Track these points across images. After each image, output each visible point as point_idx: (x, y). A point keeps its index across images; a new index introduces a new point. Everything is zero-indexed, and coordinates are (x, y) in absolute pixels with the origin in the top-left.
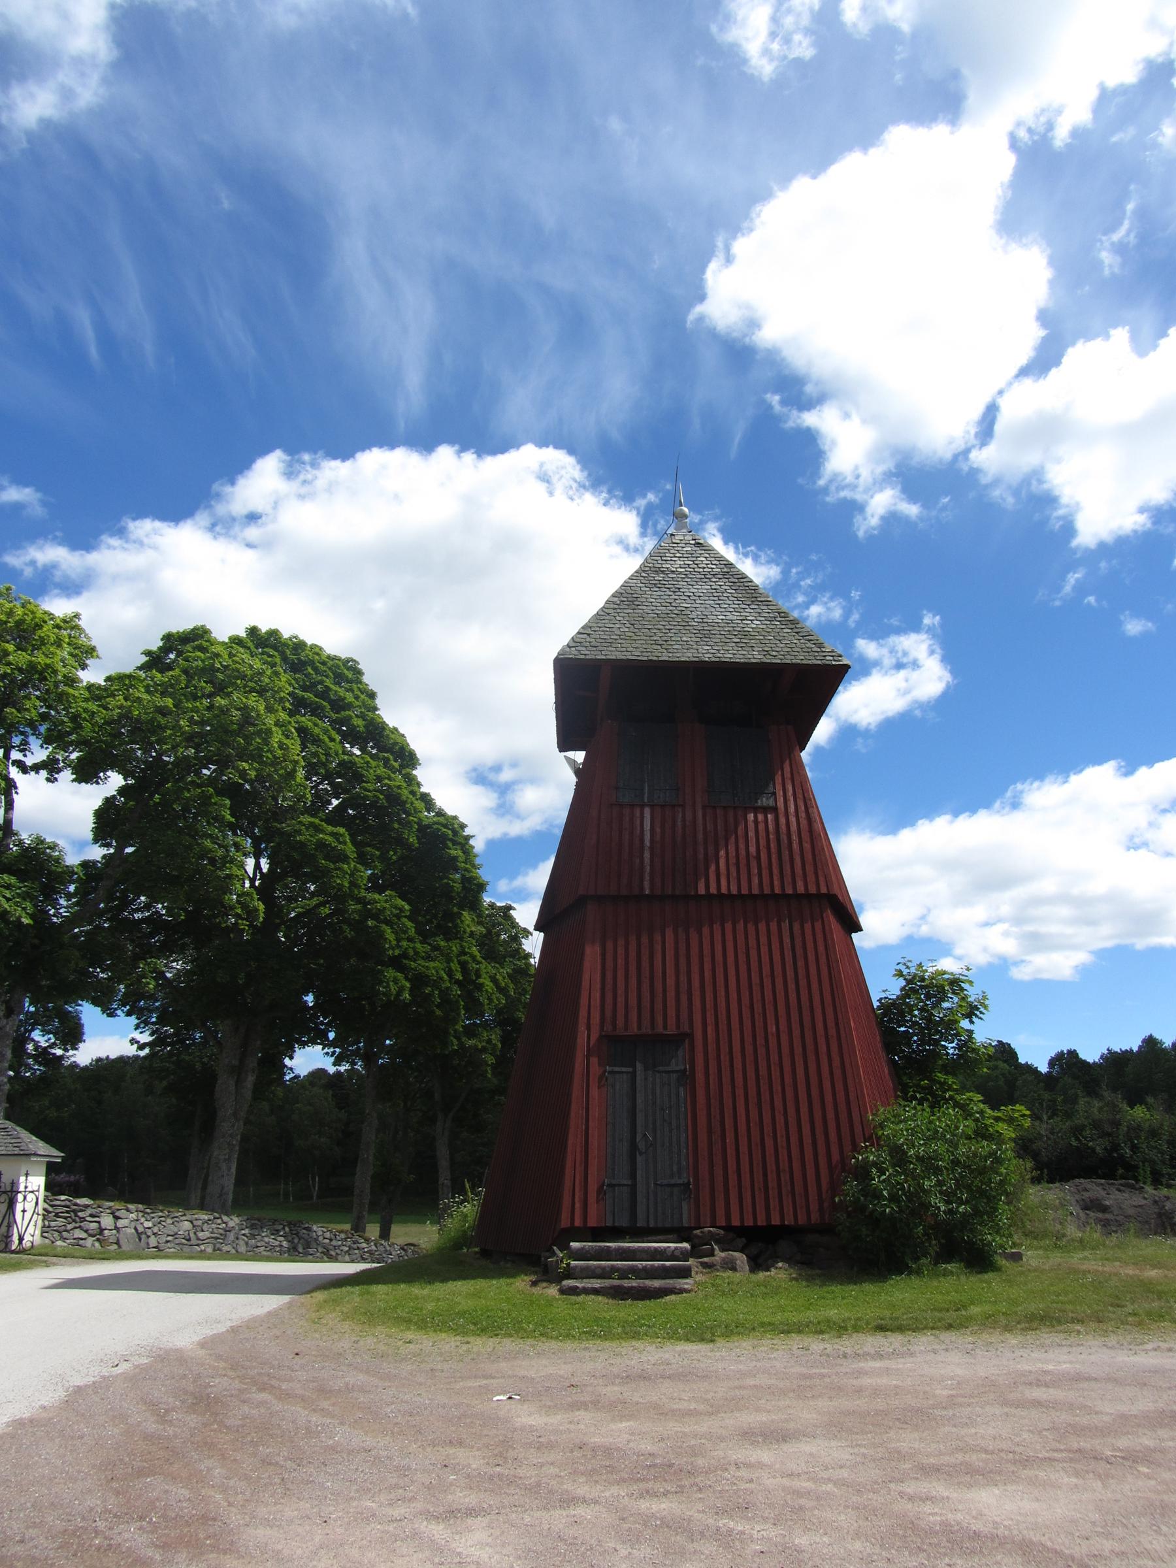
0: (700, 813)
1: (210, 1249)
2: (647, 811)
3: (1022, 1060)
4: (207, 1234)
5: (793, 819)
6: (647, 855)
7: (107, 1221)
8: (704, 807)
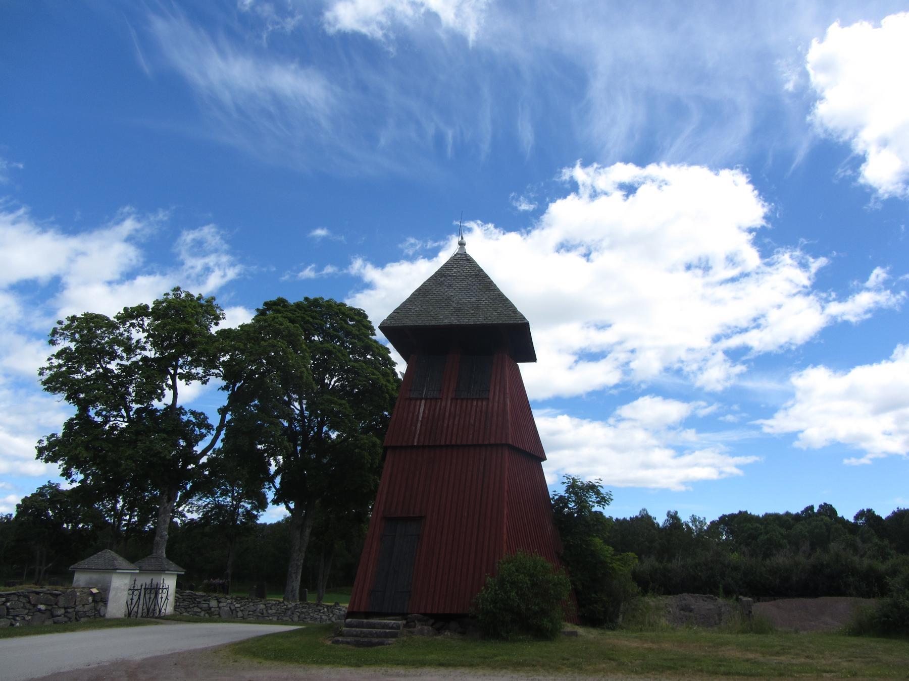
0: (449, 402)
1: (275, 619)
2: (423, 402)
3: (839, 515)
4: (274, 611)
5: (496, 404)
6: (419, 425)
7: (213, 603)
8: (452, 399)
